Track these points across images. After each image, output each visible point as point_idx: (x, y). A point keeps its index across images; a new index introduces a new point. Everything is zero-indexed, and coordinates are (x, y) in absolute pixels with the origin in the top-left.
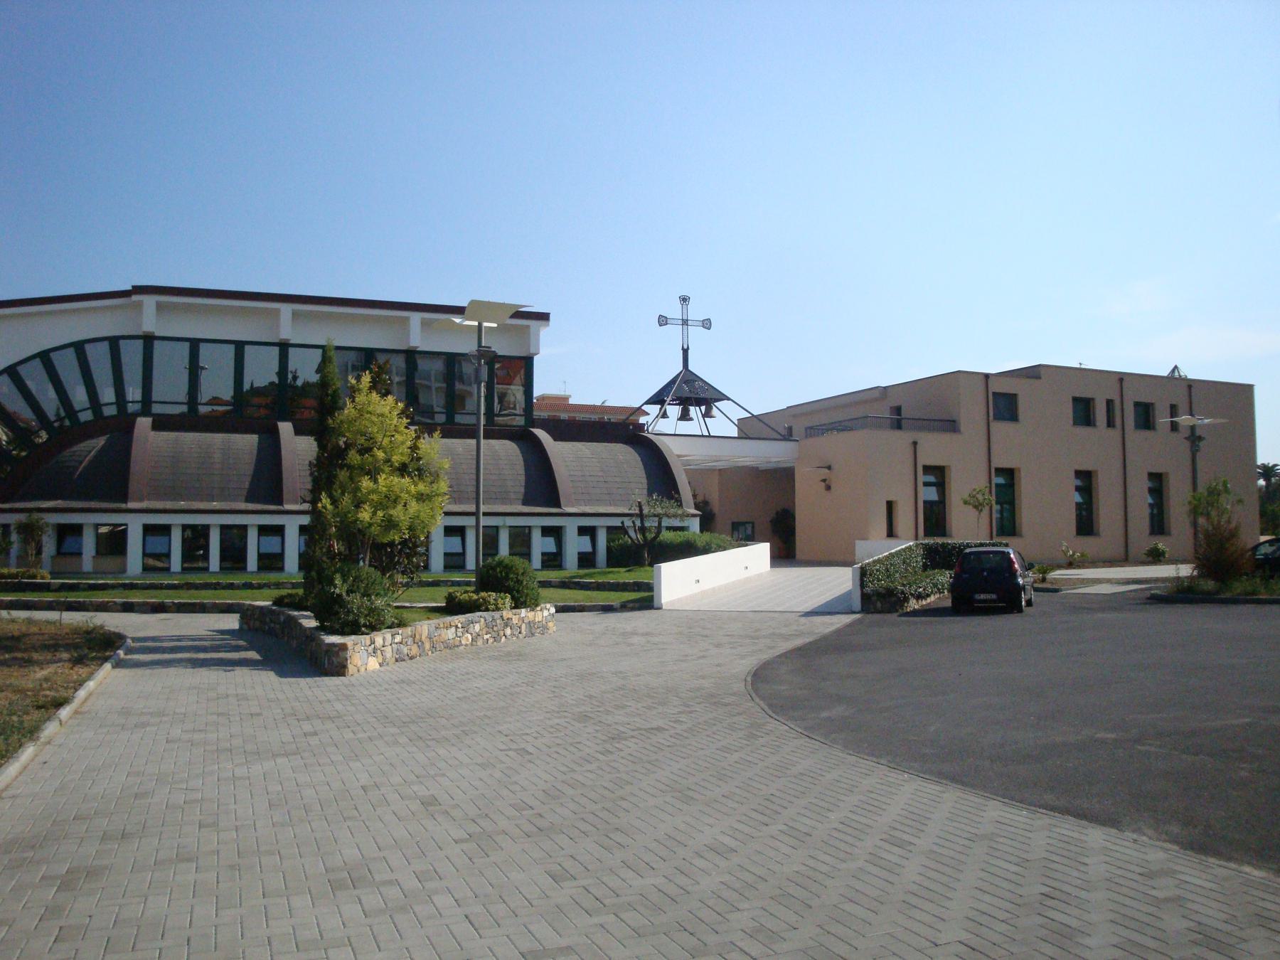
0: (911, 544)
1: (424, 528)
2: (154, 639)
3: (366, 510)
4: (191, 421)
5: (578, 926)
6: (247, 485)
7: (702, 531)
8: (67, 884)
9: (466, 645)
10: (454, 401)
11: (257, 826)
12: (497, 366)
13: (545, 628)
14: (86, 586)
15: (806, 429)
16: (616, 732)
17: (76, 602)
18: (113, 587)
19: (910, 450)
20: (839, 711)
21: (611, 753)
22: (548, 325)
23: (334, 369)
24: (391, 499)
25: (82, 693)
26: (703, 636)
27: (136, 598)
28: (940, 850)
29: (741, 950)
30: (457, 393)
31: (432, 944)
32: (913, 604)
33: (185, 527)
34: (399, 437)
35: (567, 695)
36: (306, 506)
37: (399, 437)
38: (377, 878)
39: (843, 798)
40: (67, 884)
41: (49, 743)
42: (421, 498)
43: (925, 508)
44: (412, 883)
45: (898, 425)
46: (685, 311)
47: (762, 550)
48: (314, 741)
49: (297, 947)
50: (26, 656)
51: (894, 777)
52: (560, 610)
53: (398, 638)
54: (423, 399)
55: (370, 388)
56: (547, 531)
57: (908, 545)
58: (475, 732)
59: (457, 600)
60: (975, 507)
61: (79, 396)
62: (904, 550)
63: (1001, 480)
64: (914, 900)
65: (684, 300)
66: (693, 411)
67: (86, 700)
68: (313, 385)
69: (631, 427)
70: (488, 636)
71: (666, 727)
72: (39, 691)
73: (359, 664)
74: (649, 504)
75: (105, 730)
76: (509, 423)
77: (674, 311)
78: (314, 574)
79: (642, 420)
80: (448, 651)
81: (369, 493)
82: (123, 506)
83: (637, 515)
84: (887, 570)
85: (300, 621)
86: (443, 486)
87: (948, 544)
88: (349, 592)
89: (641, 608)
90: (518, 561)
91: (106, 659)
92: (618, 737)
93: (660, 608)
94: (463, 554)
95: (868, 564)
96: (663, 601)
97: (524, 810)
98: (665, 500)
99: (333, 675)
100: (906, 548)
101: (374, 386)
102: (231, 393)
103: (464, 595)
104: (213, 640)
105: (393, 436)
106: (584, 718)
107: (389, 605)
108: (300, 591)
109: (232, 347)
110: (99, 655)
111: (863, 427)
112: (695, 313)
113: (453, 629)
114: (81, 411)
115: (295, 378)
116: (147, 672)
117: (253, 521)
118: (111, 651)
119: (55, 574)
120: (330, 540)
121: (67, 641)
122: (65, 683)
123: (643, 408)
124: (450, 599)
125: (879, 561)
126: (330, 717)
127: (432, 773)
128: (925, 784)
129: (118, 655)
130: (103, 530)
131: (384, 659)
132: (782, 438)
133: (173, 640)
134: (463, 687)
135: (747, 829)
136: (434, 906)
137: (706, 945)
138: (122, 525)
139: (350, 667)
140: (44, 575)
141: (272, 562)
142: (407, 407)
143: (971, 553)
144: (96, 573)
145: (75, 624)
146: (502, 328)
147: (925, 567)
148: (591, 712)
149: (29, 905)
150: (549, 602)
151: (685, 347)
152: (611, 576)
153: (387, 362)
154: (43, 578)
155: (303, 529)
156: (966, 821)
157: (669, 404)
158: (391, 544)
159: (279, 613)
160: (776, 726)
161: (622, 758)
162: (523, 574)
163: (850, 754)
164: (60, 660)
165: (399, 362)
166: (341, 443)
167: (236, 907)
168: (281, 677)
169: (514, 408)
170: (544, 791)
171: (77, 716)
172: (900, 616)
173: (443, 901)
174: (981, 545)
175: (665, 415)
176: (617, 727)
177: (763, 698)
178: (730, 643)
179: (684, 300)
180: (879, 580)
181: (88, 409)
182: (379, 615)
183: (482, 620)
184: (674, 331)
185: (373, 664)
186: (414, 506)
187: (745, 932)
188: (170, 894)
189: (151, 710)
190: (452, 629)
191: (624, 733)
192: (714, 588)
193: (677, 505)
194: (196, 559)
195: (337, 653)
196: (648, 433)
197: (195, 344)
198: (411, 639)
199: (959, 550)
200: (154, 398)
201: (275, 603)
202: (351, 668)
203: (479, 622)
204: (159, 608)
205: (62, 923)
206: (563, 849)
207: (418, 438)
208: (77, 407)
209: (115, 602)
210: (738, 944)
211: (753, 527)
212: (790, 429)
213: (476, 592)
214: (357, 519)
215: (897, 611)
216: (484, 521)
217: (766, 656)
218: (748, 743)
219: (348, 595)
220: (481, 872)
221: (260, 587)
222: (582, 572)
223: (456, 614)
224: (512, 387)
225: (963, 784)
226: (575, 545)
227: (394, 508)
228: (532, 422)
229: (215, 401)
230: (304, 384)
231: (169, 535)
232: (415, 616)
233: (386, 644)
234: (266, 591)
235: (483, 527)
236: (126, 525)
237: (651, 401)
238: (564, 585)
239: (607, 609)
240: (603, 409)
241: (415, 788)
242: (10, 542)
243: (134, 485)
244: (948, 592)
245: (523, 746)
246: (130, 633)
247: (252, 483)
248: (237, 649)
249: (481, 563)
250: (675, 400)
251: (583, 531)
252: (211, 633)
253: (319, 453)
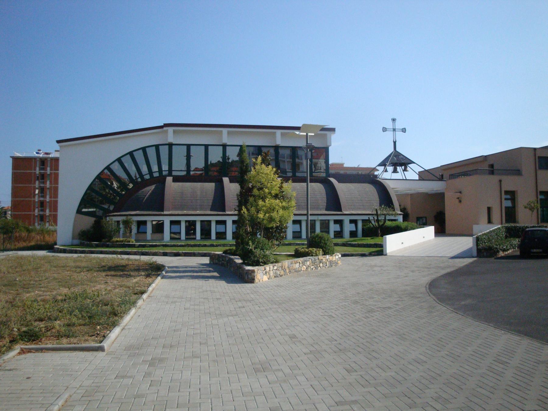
0: (500, 226)
1: (286, 221)
2: (176, 267)
3: (261, 214)
4: (187, 178)
5: (359, 391)
6: (211, 204)
7: (404, 221)
8: (152, 363)
9: (304, 271)
10: (295, 167)
11: (223, 345)
12: (313, 151)
13: (337, 263)
14: (149, 246)
15: (450, 175)
16: (370, 309)
17: (145, 252)
18: (159, 246)
19: (498, 184)
20: (469, 301)
21: (369, 318)
22: (335, 133)
23: (246, 155)
24: (272, 209)
25: (150, 289)
26: (406, 267)
27: (168, 250)
28: (522, 367)
29: (432, 406)
30: (297, 163)
31: (297, 396)
32: (501, 254)
33: (186, 221)
34: (274, 183)
35: (348, 292)
36: (236, 212)
37: (274, 183)
38: (274, 368)
39: (473, 340)
40: (152, 363)
41: (140, 308)
42: (284, 208)
43: (506, 210)
44: (287, 371)
45: (492, 172)
46: (394, 125)
47: (431, 229)
48: (243, 310)
49: (243, 395)
50: (128, 273)
51: (497, 332)
52: (343, 255)
53: (275, 268)
54: (282, 166)
55: (262, 163)
56: (336, 222)
57: (498, 227)
58: (310, 308)
59: (299, 251)
60: (530, 209)
61: (144, 169)
62: (496, 229)
63: (542, 197)
64: (511, 389)
65: (394, 120)
66: (399, 168)
67: (152, 291)
68: (236, 161)
70: (313, 267)
71: (392, 307)
72: (134, 287)
73: (260, 278)
74: (380, 210)
75: (160, 304)
76: (319, 176)
77: (390, 125)
78: (239, 240)
79: (376, 173)
80: (296, 273)
81: (262, 207)
82: (162, 213)
83: (375, 214)
84: (489, 238)
85: (235, 260)
86: (293, 203)
87: (517, 226)
88: (255, 248)
89: (378, 255)
90: (325, 235)
91: (159, 275)
92: (371, 311)
93: (386, 255)
94: (300, 232)
95: (480, 235)
96: (387, 252)
97: (333, 341)
98: (387, 208)
99: (248, 283)
100: (497, 228)
101: (263, 161)
102: (203, 165)
103: (302, 249)
104: (199, 268)
105: (272, 182)
106: (356, 302)
107: (271, 253)
108: (234, 248)
109: (221, 147)
110: (156, 273)
111: (476, 174)
112: (399, 126)
113: (298, 264)
114: (145, 175)
115: (229, 159)
116: (174, 280)
117: (213, 219)
118: (160, 272)
119: (137, 241)
120: (246, 226)
121: (143, 268)
122: (144, 284)
123: (376, 168)
124: (296, 251)
125: (485, 234)
126: (249, 300)
127: (293, 325)
128: (512, 336)
129: (163, 273)
130: (154, 223)
131: (270, 277)
133: (192, 268)
134: (303, 288)
135: (430, 353)
136: (298, 380)
137: (415, 403)
138: (162, 221)
139: (256, 279)
140: (133, 241)
141: (221, 235)
142: (277, 170)
143: (529, 231)
144: (152, 240)
145: (146, 261)
146: (316, 135)
147: (506, 237)
148: (359, 300)
149: (139, 371)
150: (338, 252)
151: (395, 141)
152: (364, 241)
153: (268, 151)
154: (132, 242)
155: (234, 222)
156: (533, 354)
157: (388, 166)
158: (272, 228)
159: (226, 257)
160: (441, 308)
161: (374, 320)
162: (327, 240)
163: (476, 321)
164: (141, 275)
165: (272, 151)
166: (250, 186)
167: (217, 377)
168: (228, 283)
169: (321, 169)
170: (341, 333)
171: (149, 298)
172: (495, 259)
173: (301, 379)
174: (533, 227)
175: (386, 171)
176: (370, 306)
177: (434, 295)
178: (418, 270)
179: (394, 120)
180: (485, 243)
181: (148, 174)
182: (267, 258)
183: (310, 260)
184: (390, 134)
185: (265, 278)
186: (281, 212)
187: (432, 398)
188: (191, 370)
189: (177, 296)
190: (298, 263)
191: (373, 309)
192: (409, 246)
194: (190, 234)
195: (251, 274)
196: (379, 179)
197: (189, 146)
198: (281, 268)
199: (523, 229)
200: (173, 169)
201: (224, 253)
202: (256, 280)
203: (309, 261)
204: (177, 255)
205: (152, 379)
206: (350, 359)
207: (282, 183)
208: (144, 173)
209: (160, 252)
210: (430, 403)
211: (426, 219)
212: (442, 176)
213: (308, 248)
214: (258, 218)
215: (493, 257)
216: (310, 218)
217: (434, 276)
218: (428, 314)
219: (255, 250)
220: (316, 367)
221: (217, 246)
222: (352, 239)
223: (299, 257)
224: (320, 160)
225: (530, 336)
226: (348, 228)
227: (273, 213)
228: (329, 175)
229: (196, 169)
230: (232, 161)
231: (180, 225)
232: (282, 258)
233: (271, 270)
234: (219, 248)
235: (310, 220)
236: (163, 221)
237: (380, 165)
238: (344, 245)
239: (363, 255)
240: (358, 169)
241: (286, 331)
242: (120, 228)
243: (167, 203)
244: (518, 248)
245: (330, 314)
246: (167, 265)
247: (213, 203)
248: (210, 271)
249: (309, 236)
251: (352, 221)
252: (198, 265)
253: (241, 190)
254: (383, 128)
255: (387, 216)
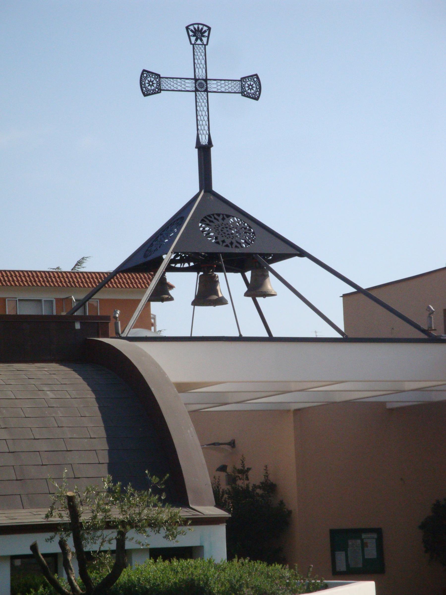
7: (230, 557)
46: (200, 60)
69: (78, 326)
98: (130, 489)
132: (423, 336)
151: (204, 141)
193: (160, 499)
250: (182, 261)
254: (145, 73)
255: (131, 533)
